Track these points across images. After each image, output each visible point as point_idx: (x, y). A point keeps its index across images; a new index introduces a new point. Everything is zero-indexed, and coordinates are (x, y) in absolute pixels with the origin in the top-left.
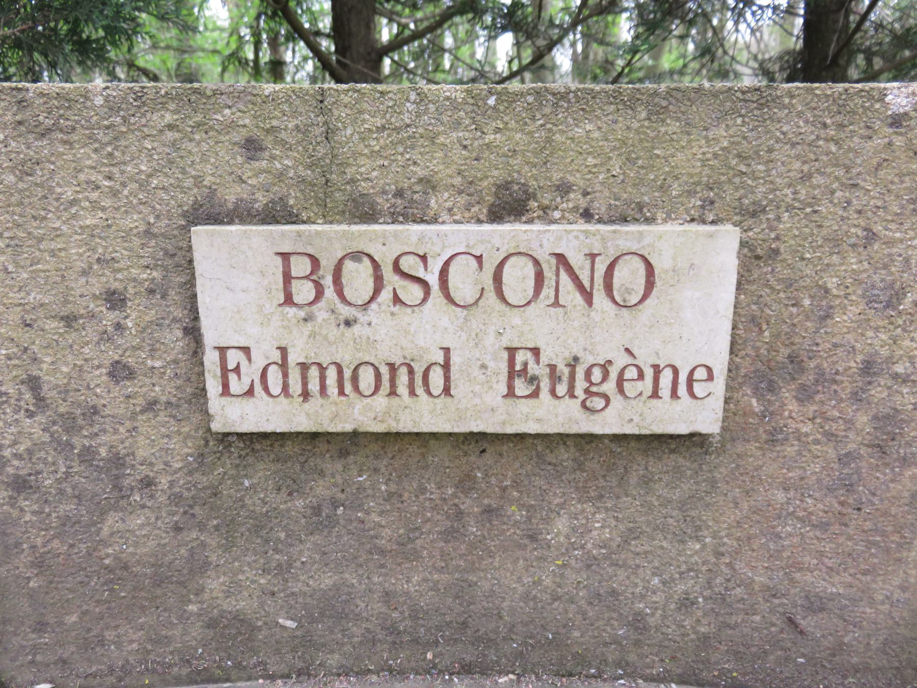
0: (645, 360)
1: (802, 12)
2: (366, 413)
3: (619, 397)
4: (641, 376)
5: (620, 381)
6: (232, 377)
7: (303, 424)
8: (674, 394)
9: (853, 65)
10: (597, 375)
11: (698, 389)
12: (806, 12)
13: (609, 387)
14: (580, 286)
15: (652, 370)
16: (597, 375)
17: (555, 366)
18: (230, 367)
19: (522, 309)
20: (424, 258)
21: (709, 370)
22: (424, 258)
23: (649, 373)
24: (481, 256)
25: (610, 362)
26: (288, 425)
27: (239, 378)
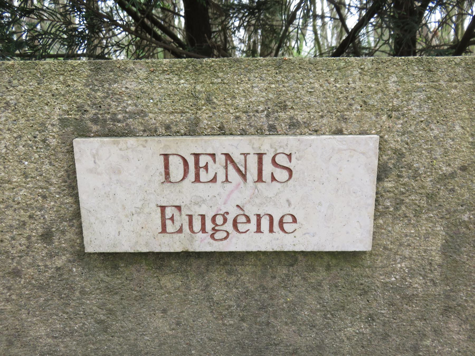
0: (251, 211)
1: (182, 13)
2: (203, 244)
3: (235, 232)
4: (249, 221)
5: (235, 224)
6: (168, 222)
7: (178, 249)
8: (271, 230)
9: (417, 43)
10: (219, 220)
11: (240, 227)
12: (185, 13)
13: (229, 226)
14: (239, 171)
15: (255, 217)
16: (219, 220)
17: (204, 215)
18: (167, 217)
19: (285, 184)
21: (247, 217)
22: (289, 156)
23: (254, 220)
25: (227, 213)
26: (107, 248)
27: (173, 223)
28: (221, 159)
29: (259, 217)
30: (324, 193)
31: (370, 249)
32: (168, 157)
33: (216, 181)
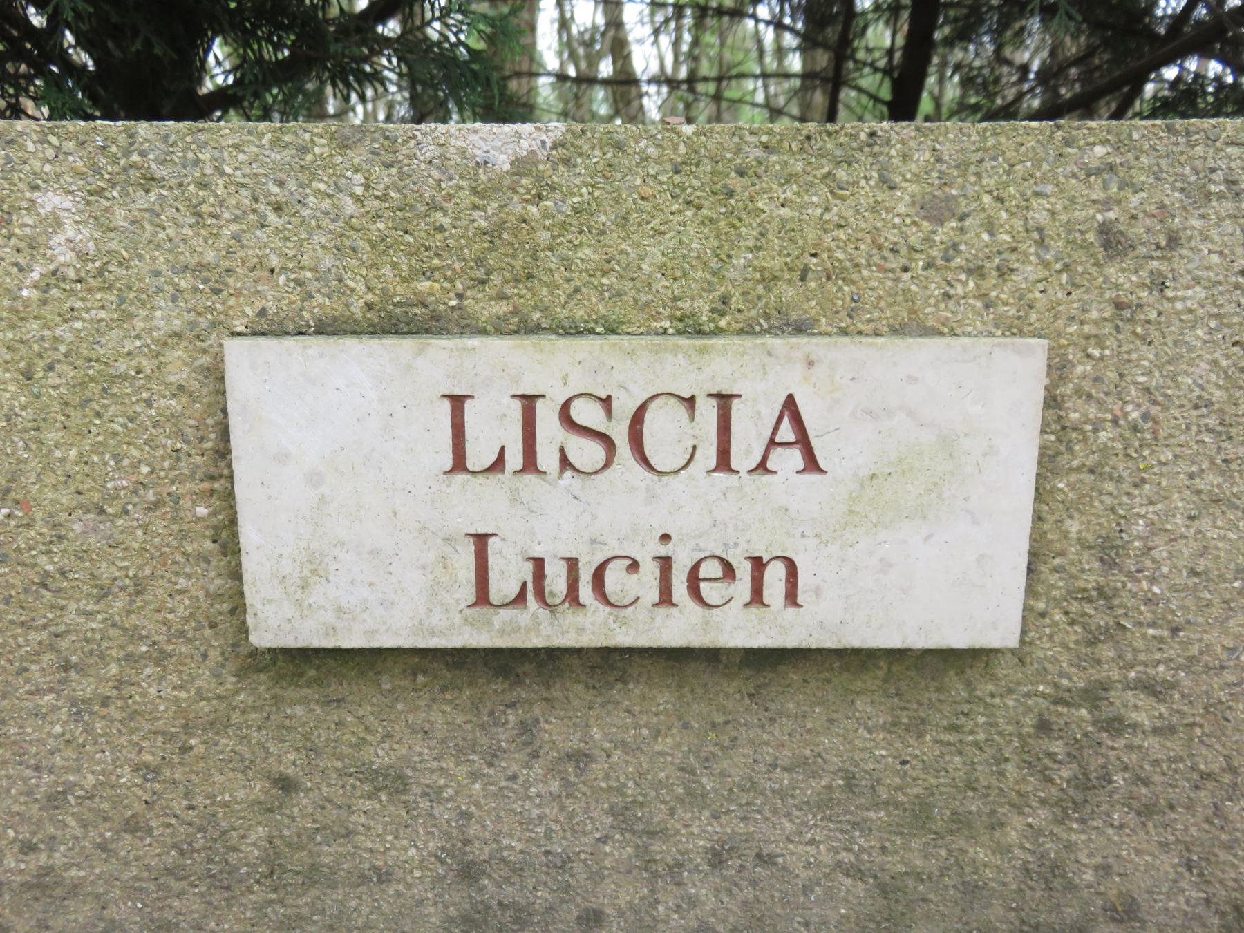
4: (729, 571)
15: (748, 566)
20: (607, 402)
22: (607, 402)
23: (744, 571)
24: (609, 397)
28: (708, 412)
29: (758, 565)
30: (898, 475)
31: (1013, 641)
32: (463, 404)
33: (503, 471)
